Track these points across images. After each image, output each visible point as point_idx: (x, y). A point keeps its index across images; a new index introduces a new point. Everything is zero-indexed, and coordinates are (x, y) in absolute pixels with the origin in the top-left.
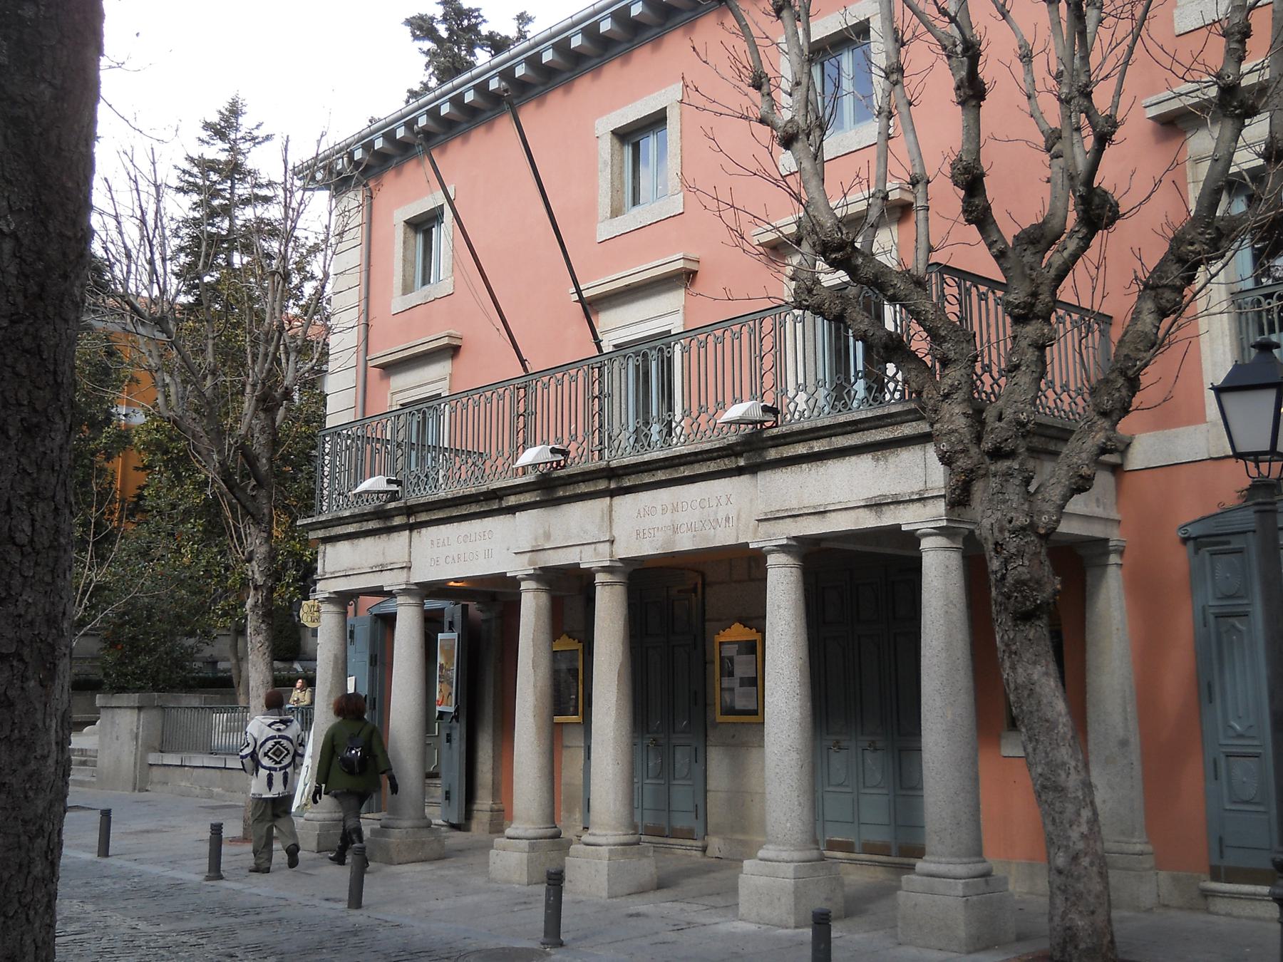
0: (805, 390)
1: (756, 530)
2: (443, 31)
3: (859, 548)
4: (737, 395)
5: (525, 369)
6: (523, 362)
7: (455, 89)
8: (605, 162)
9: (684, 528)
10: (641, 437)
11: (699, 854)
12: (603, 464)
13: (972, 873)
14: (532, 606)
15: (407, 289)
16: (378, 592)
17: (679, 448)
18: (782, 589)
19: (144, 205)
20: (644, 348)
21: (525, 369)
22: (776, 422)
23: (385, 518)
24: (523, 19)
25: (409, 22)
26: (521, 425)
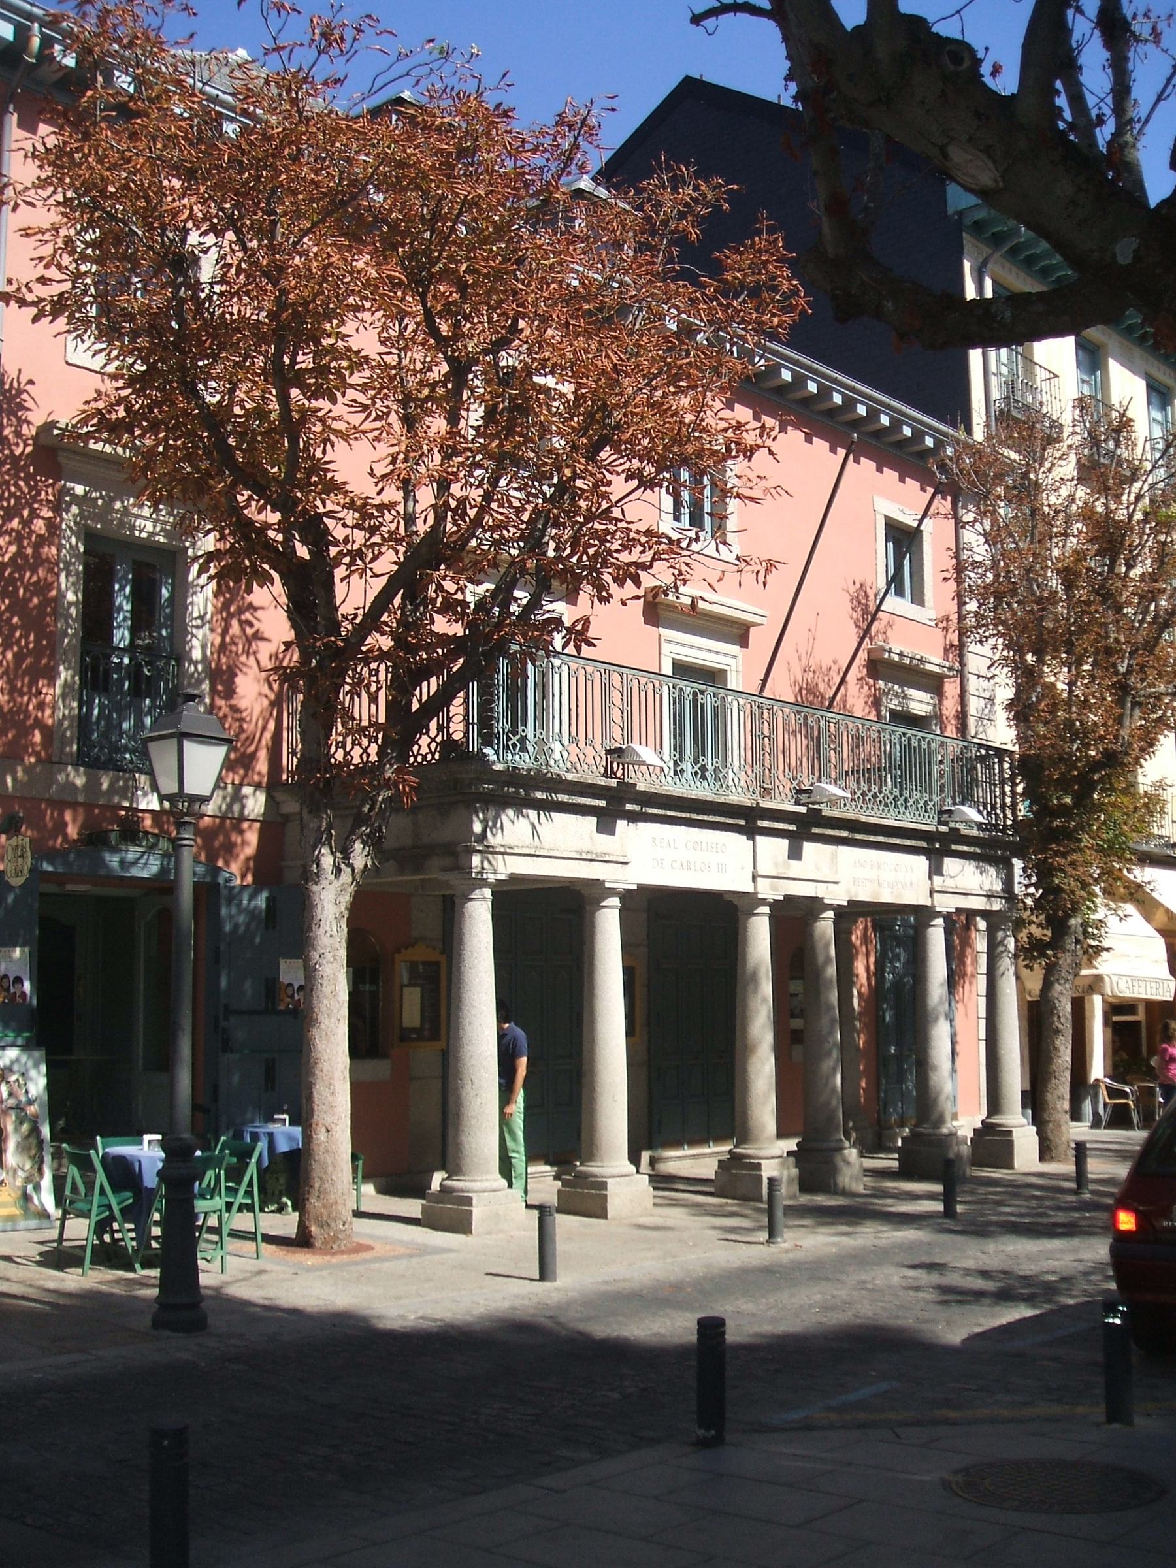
5: (761, 691)
6: (764, 681)
18: (609, 927)
21: (761, 691)
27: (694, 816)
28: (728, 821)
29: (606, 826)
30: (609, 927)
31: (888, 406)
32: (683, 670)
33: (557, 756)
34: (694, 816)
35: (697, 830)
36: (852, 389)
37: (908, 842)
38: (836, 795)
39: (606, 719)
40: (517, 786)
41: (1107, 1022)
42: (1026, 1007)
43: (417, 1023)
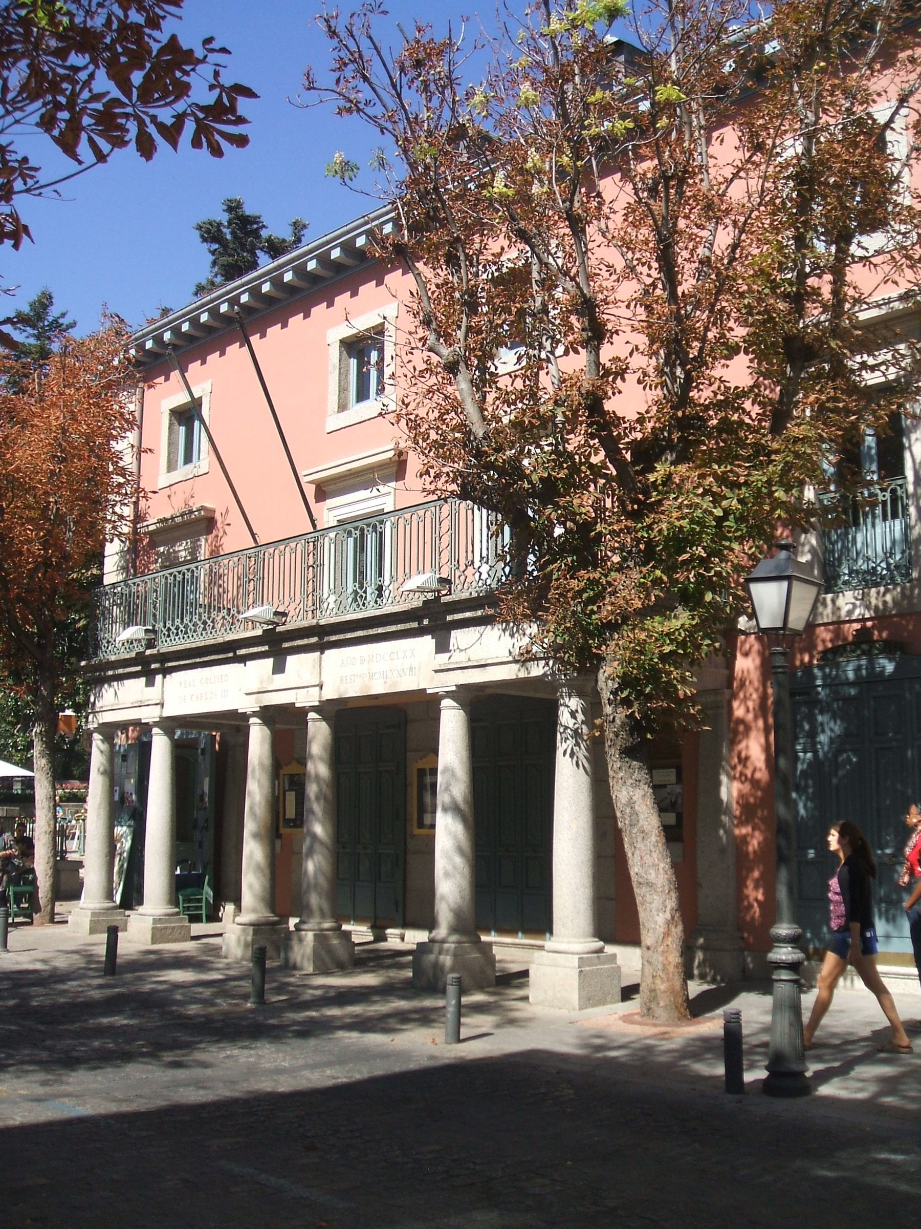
0: (487, 563)
1: (432, 679)
2: (228, 234)
3: (513, 693)
4: (421, 568)
5: (314, 526)
6: (253, 535)
7: (212, 301)
8: (334, 365)
9: (377, 676)
10: (358, 598)
11: (398, 940)
12: (314, 622)
13: (587, 950)
14: (258, 741)
15: (171, 467)
16: (137, 723)
17: (388, 608)
18: (452, 725)
19: (392, 74)
20: (360, 524)
21: (314, 526)
22: (450, 590)
23: (150, 666)
24: (298, 227)
25: (200, 228)
26: (310, 576)
27: (198, 660)
28: (220, 657)
29: (150, 683)
30: (452, 725)
34: (198, 660)
35: (189, 672)
37: (393, 628)
39: (436, 552)
40: (100, 671)
43: (293, 817)
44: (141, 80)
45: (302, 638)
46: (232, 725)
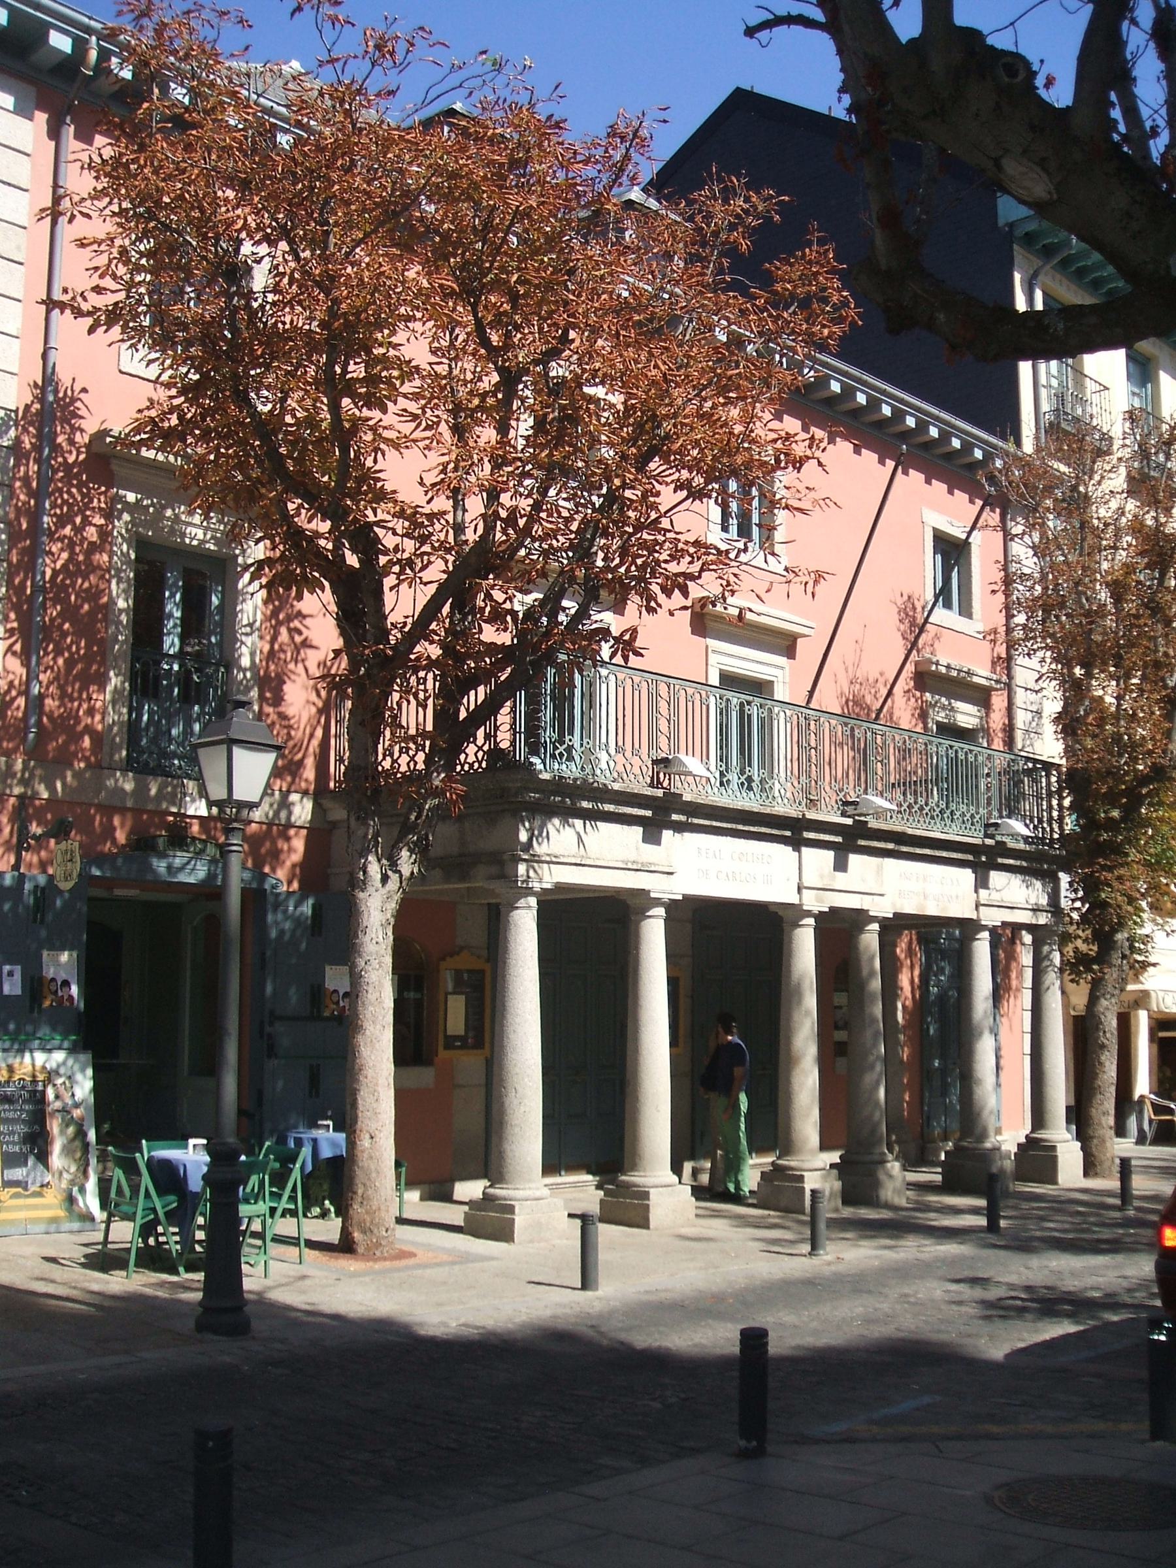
5: (809, 702)
21: (809, 702)
27: (740, 827)
31: (937, 419)
32: (729, 680)
33: (604, 766)
34: (740, 827)
36: (901, 401)
38: (882, 808)
41: (1152, 1037)
42: (1071, 1021)
44: (999, 46)
45: (879, 840)
46: (765, 925)
